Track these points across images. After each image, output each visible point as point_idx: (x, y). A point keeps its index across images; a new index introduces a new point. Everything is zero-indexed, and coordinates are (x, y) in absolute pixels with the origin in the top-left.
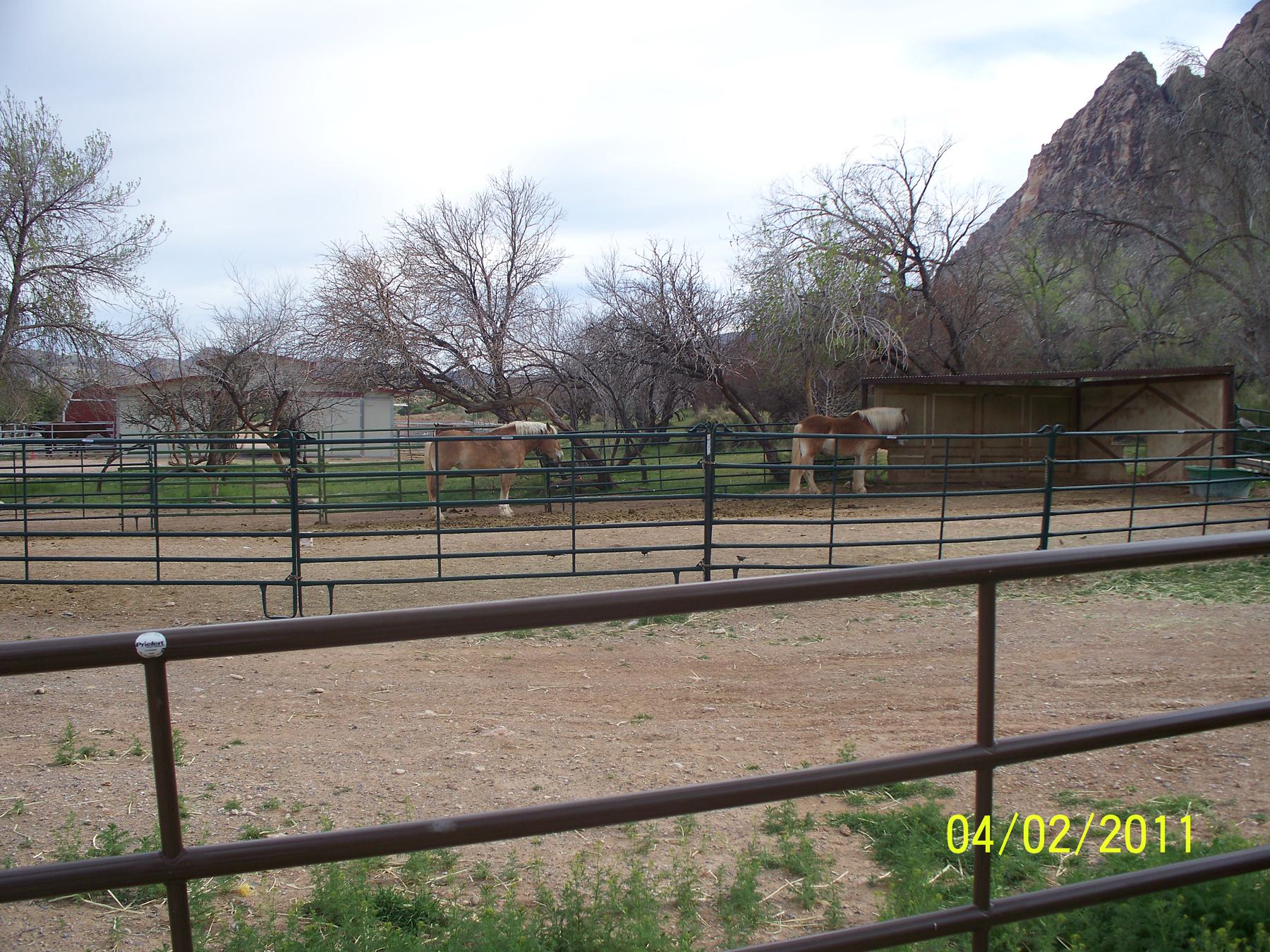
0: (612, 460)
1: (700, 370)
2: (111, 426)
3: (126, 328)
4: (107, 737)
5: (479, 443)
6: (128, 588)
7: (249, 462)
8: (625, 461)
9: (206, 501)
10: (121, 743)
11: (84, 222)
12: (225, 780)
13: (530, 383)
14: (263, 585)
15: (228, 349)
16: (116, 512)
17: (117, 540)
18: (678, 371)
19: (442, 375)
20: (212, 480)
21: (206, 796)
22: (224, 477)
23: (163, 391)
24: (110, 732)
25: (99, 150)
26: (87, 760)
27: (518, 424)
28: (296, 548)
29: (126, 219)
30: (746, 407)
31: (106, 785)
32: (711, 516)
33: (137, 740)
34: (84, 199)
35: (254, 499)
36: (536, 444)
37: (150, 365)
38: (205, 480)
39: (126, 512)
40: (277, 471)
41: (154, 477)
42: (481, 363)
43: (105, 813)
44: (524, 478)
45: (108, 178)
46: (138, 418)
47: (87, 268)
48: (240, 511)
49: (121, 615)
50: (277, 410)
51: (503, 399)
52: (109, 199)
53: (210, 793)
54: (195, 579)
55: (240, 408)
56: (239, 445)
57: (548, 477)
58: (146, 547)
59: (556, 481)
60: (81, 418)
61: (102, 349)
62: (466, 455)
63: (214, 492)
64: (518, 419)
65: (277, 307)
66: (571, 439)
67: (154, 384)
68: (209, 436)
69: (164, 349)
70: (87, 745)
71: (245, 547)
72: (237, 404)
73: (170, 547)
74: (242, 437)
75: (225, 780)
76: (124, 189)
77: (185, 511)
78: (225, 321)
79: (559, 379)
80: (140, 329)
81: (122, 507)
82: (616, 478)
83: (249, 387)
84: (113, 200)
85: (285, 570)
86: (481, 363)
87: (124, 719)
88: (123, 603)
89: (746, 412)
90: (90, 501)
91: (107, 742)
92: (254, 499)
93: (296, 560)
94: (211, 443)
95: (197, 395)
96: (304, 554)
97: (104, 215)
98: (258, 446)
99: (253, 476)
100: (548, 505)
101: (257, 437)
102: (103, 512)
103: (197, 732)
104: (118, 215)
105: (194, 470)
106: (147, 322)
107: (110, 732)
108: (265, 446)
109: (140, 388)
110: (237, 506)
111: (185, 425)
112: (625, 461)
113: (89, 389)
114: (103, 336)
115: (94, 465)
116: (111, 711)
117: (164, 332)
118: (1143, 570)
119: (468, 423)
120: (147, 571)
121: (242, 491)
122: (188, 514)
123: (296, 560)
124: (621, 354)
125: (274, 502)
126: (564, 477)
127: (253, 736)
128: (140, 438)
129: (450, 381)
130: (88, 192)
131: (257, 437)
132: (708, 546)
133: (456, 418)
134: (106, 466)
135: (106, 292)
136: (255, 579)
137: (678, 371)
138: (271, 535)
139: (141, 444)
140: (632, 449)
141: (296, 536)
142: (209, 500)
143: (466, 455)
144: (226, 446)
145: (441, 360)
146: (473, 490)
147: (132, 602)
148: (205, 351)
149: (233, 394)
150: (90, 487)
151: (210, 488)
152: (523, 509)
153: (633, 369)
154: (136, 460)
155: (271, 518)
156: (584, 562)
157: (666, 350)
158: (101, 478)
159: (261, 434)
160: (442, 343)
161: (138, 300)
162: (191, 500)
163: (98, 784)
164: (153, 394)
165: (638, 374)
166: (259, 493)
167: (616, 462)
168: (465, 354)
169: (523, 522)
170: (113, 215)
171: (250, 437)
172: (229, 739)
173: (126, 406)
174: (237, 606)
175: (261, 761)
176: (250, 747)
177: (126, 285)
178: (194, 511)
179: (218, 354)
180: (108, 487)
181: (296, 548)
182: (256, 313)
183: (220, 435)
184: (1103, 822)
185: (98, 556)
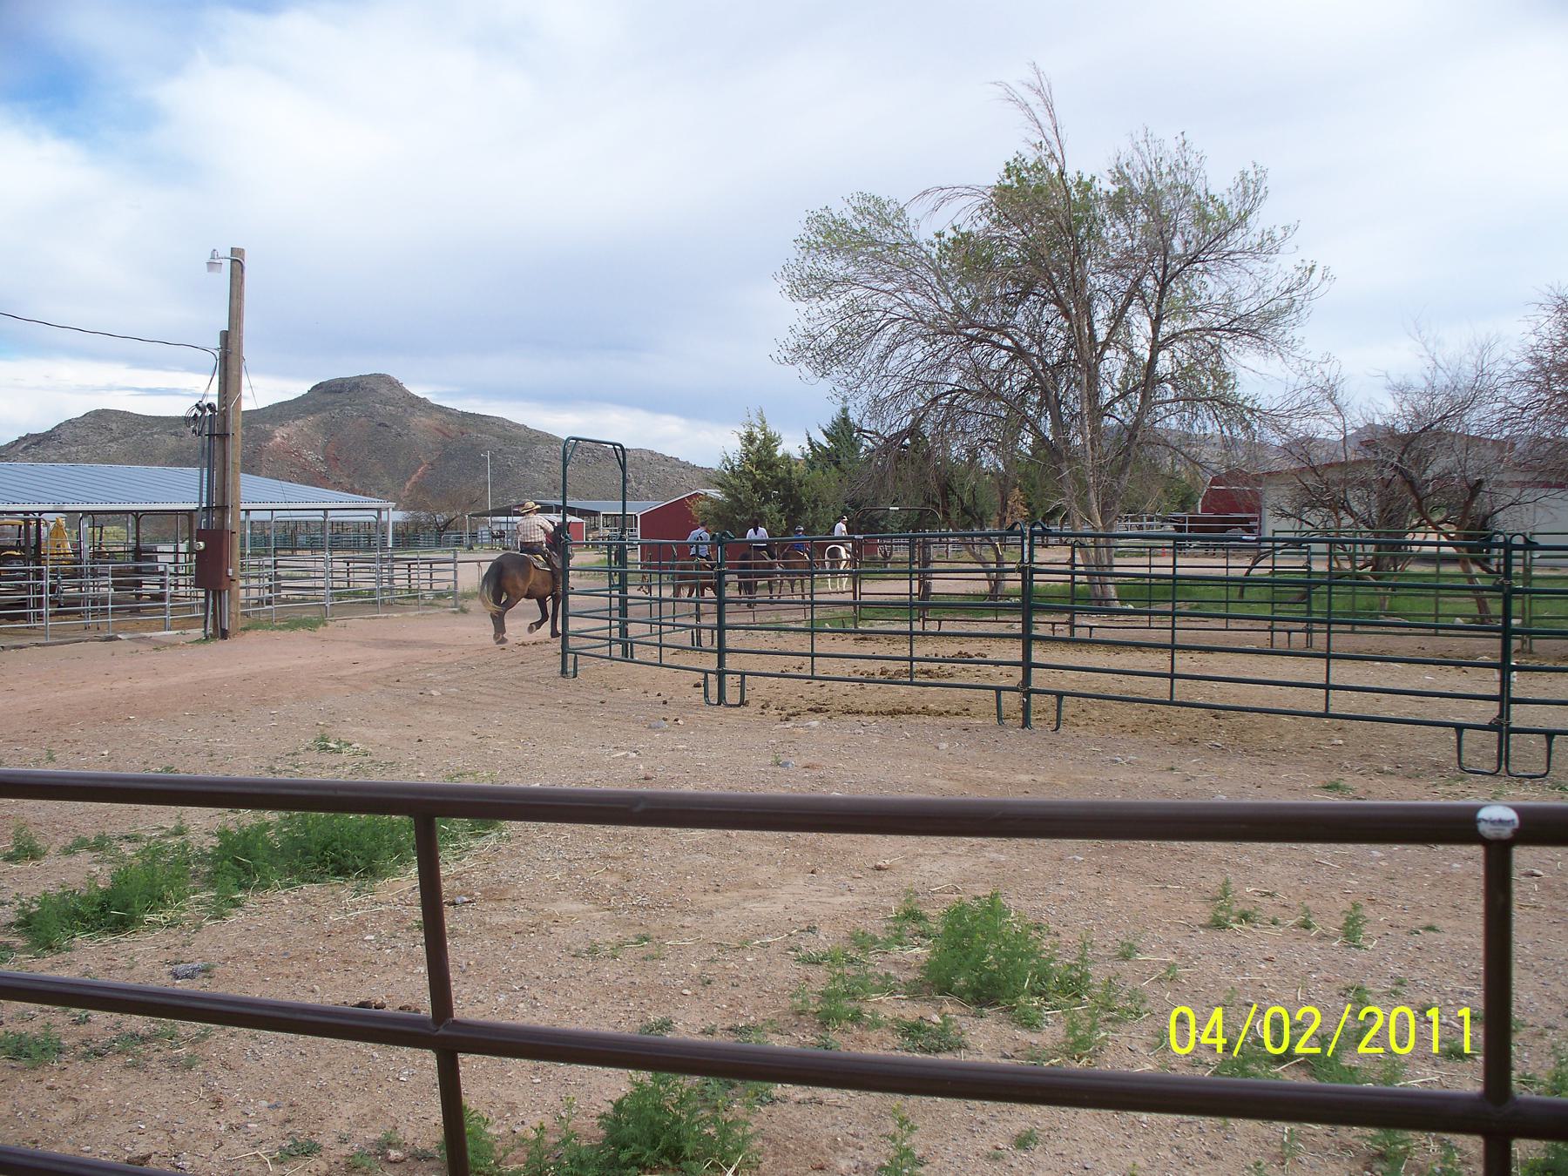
2: (1255, 519)
3: (1280, 401)
4: (1267, 900)
6: (1286, 719)
7: (1429, 569)
9: (1371, 616)
10: (1285, 911)
11: (1231, 275)
12: (1417, 975)
14: (1460, 728)
15: (1403, 428)
16: (1265, 625)
17: (1266, 658)
20: (1381, 590)
21: (1394, 992)
22: (1394, 587)
23: (1321, 478)
24: (1271, 895)
25: (1251, 190)
26: (1245, 927)
28: (1027, 653)
29: (1282, 268)
31: (1270, 960)
33: (1307, 910)
34: (1231, 248)
35: (1437, 616)
37: (1302, 447)
38: (1371, 590)
39: (1278, 625)
40: (1464, 582)
41: (1307, 585)
43: (1270, 994)
45: (1260, 222)
46: (1289, 510)
47: (1234, 330)
48: (1414, 630)
49: (1278, 751)
50: (1468, 504)
52: (1261, 246)
53: (1399, 989)
54: (1366, 714)
55: (1420, 501)
56: (1416, 548)
58: (1313, 670)
60: (1223, 513)
61: (1249, 426)
63: (1382, 605)
65: (1469, 372)
67: (1314, 469)
68: (1377, 535)
69: (1326, 427)
70: (1247, 908)
71: (1426, 678)
72: (1417, 495)
73: (1343, 673)
74: (1419, 537)
75: (1417, 975)
76: (1279, 234)
77: (1348, 628)
78: (1401, 390)
80: (1297, 403)
81: (1273, 619)
83: (1430, 474)
84: (1266, 247)
87: (1288, 881)
88: (1280, 736)
90: (1234, 610)
91: (1268, 908)
92: (1437, 616)
93: (1027, 665)
94: (1379, 545)
95: (1364, 484)
96: (729, 644)
97: (1255, 266)
98: (1443, 549)
99: (1434, 588)
101: (1443, 539)
102: (1247, 624)
103: (1379, 908)
104: (1270, 266)
105: (1359, 577)
106: (1305, 394)
107: (1271, 895)
108: (1450, 550)
109: (1294, 473)
110: (1413, 625)
111: (1348, 520)
113: (1233, 474)
114: (1251, 411)
115: (1238, 566)
116: (1272, 869)
117: (1329, 406)
120: (1313, 700)
121: (1421, 605)
122: (1353, 632)
123: (1027, 665)
125: (1459, 621)
127: (1451, 923)
128: (1291, 535)
130: (1237, 239)
131: (1443, 539)
134: (1250, 568)
135: (1257, 358)
136: (989, 683)
138: (1458, 665)
139: (1298, 543)
141: (1027, 639)
142: (1376, 616)
144: (1393, 548)
147: (1290, 737)
148: (1371, 427)
149: (1410, 482)
150: (1234, 592)
151: (1377, 600)
154: (1289, 562)
155: (1455, 642)
158: (1245, 582)
159: (1446, 535)
161: (1296, 366)
162: (1357, 615)
163: (1260, 958)
164: (1310, 480)
166: (1443, 609)
170: (1265, 265)
171: (1432, 538)
172: (1420, 923)
173: (1274, 496)
174: (1422, 752)
175: (1463, 958)
176: (1448, 936)
177: (1279, 348)
178: (1358, 628)
179: (1391, 432)
180: (1252, 593)
181: (1027, 653)
182: (1442, 380)
183: (1388, 534)
184: (1362, 1017)
185: (1248, 677)
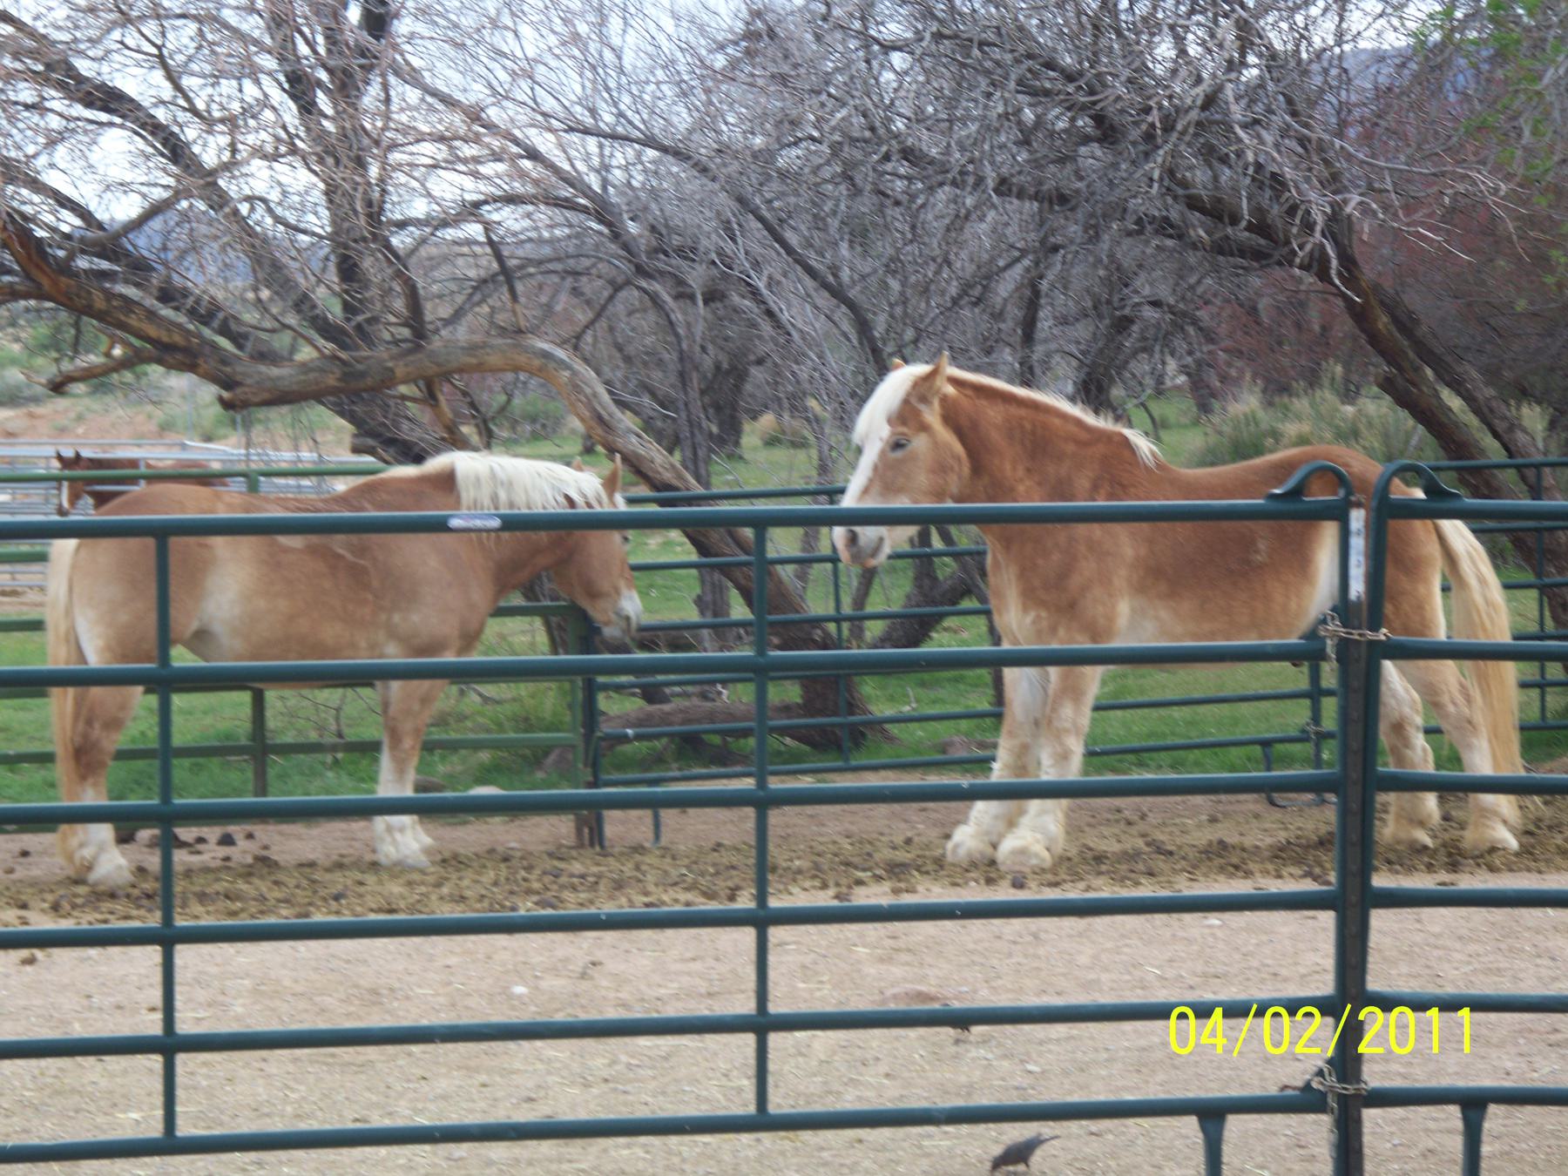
0: (858, 620)
1: (1261, 227)
5: (295, 542)
8: (915, 627)
13: (506, 275)
18: (1164, 226)
19: (109, 243)
27: (466, 463)
30: (1457, 386)
32: (1366, 871)
36: (543, 559)
42: (286, 191)
44: (474, 697)
51: (377, 345)
57: (591, 690)
59: (617, 707)
62: (230, 595)
64: (460, 443)
66: (696, 530)
79: (629, 256)
82: (880, 700)
85: (1308, 1044)
86: (286, 191)
89: (1454, 402)
100: (589, 818)
112: (915, 627)
118: (931, 805)
119: (225, 451)
124: (908, 154)
126: (652, 694)
129: (139, 268)
132: (1350, 994)
133: (162, 424)
137: (1164, 226)
140: (946, 569)
143: (230, 595)
145: (105, 176)
146: (259, 748)
152: (472, 835)
153: (961, 220)
156: (807, 1069)
157: (1107, 132)
160: (110, 100)
165: (981, 231)
167: (874, 629)
168: (210, 151)
169: (478, 892)
